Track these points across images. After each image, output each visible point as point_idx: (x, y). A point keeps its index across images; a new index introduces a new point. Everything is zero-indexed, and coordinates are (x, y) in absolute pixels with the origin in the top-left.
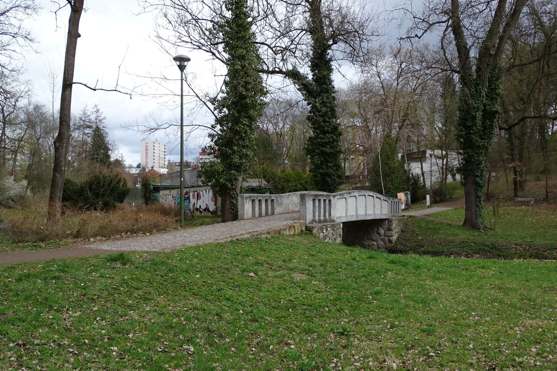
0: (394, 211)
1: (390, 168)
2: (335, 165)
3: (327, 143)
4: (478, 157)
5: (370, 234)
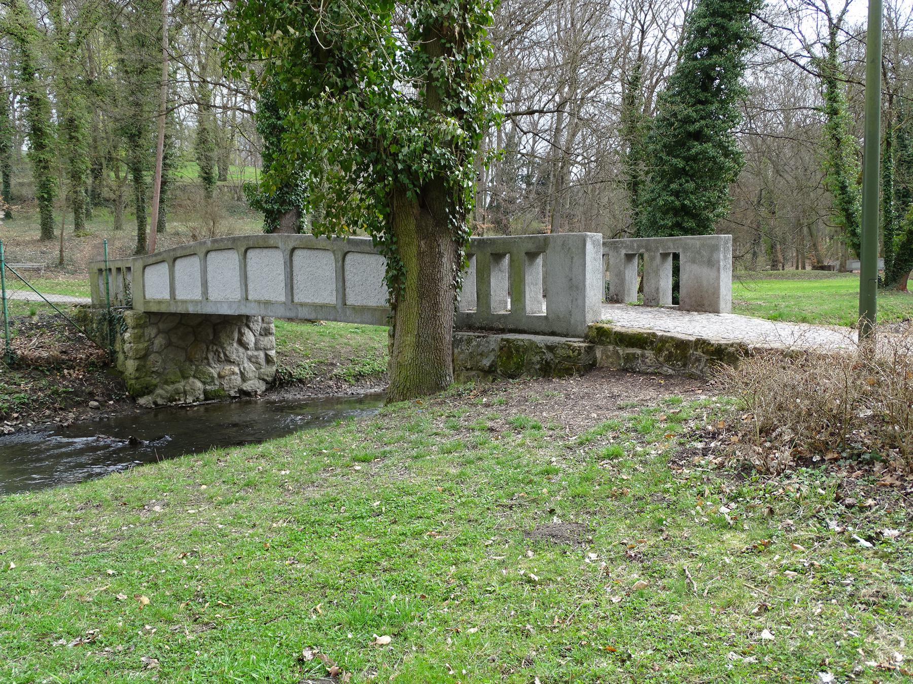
5: (223, 348)
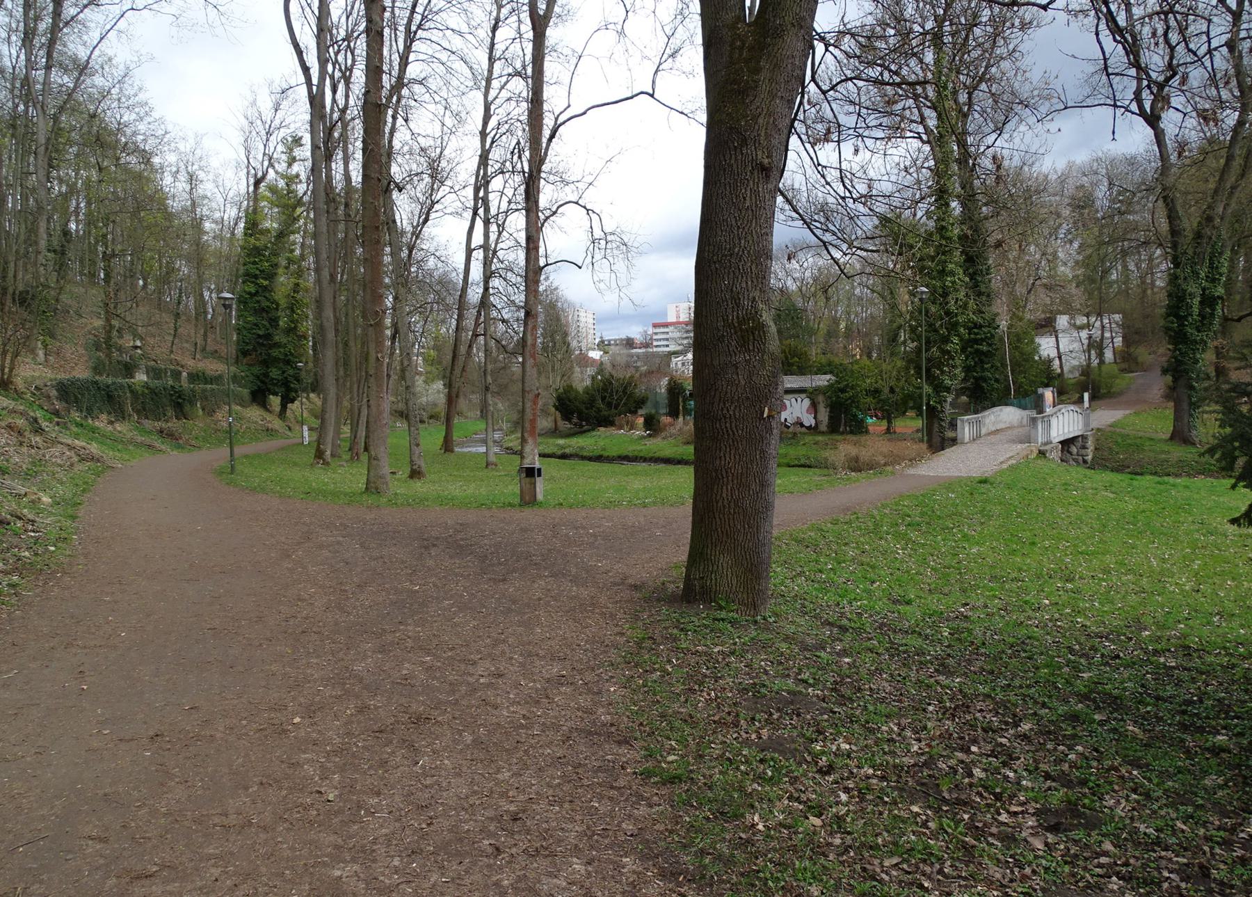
0: (664, 339)
1: (1022, 354)
2: (992, 366)
3: (982, 340)
4: (1194, 354)
